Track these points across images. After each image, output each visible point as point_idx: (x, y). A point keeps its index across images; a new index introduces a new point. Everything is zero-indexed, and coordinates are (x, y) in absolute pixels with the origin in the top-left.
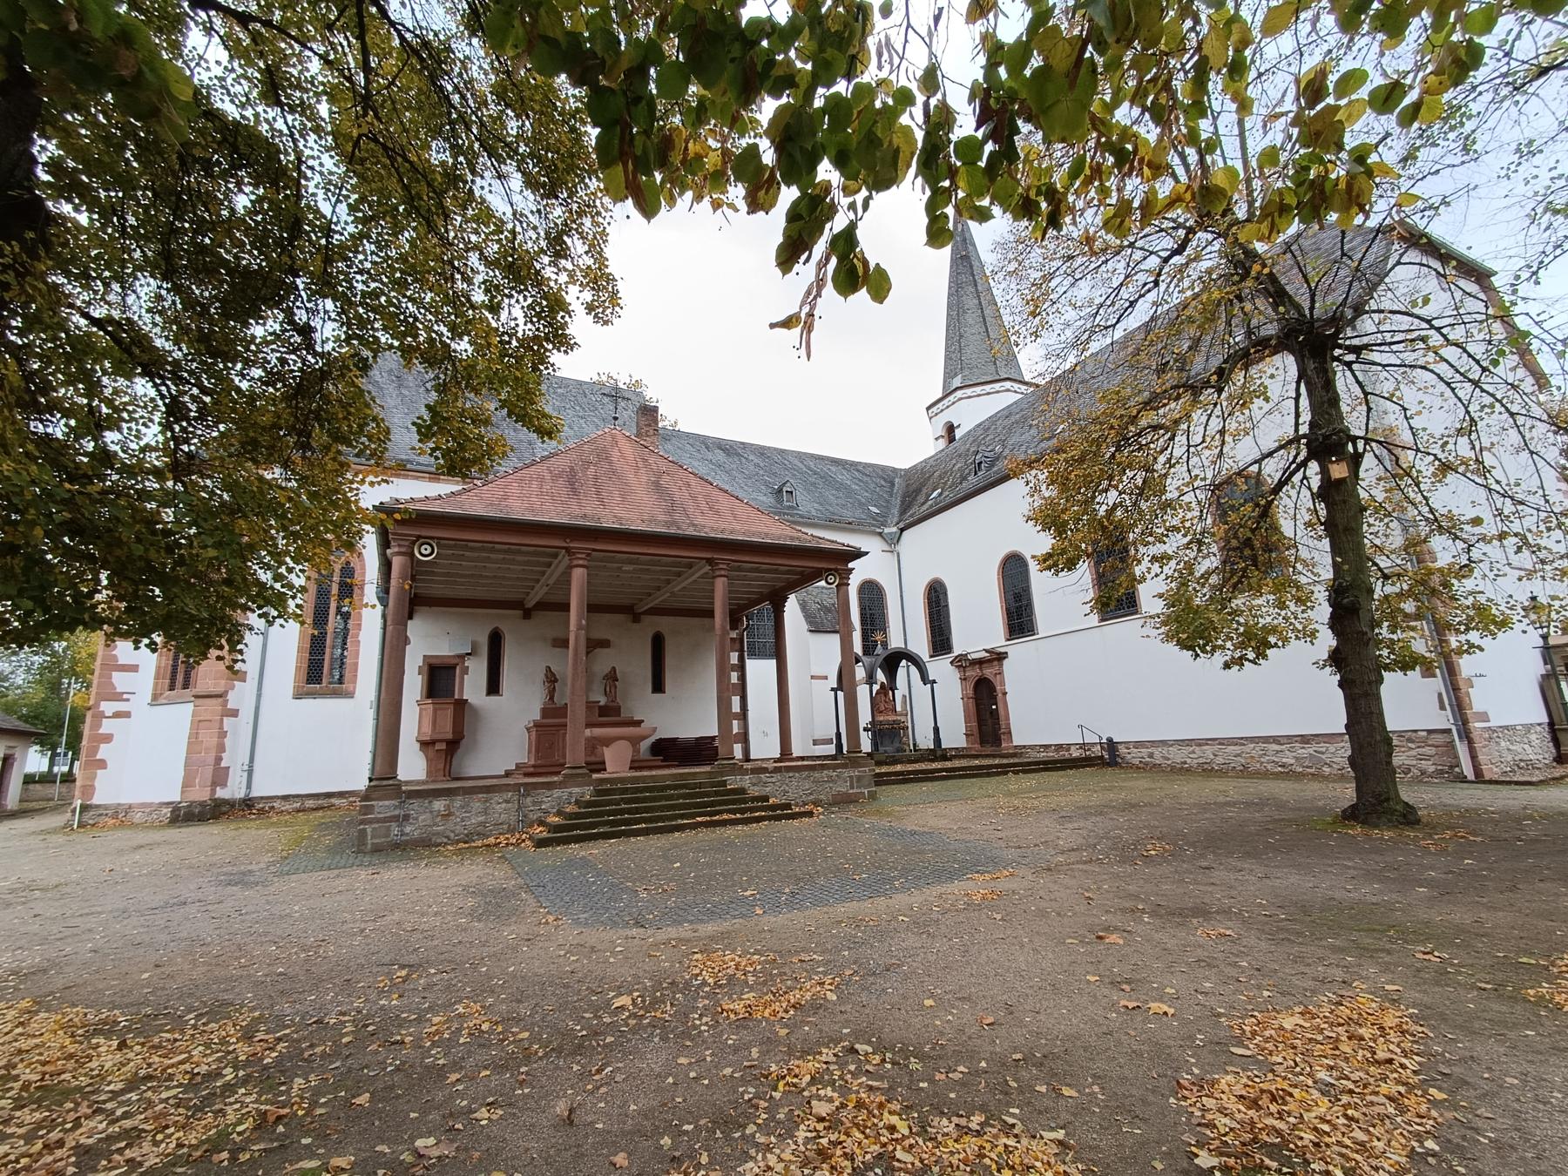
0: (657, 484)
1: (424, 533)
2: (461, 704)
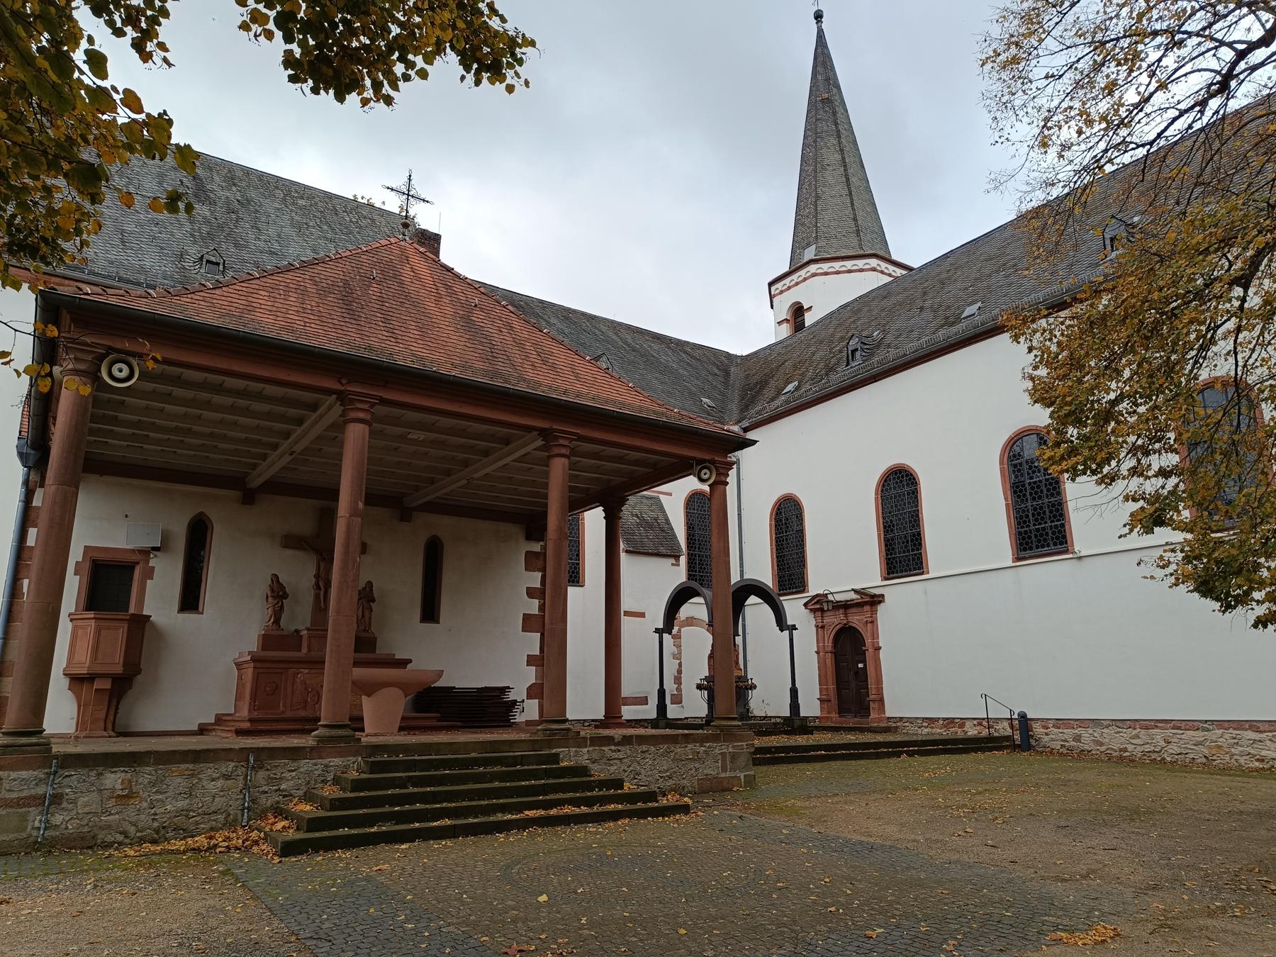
0: (467, 319)
1: (118, 345)
2: (140, 622)
